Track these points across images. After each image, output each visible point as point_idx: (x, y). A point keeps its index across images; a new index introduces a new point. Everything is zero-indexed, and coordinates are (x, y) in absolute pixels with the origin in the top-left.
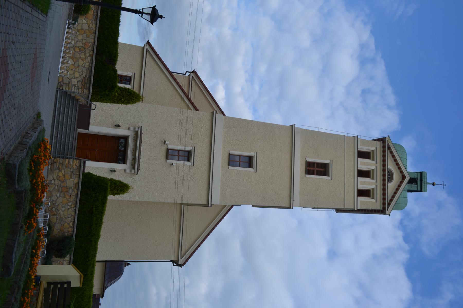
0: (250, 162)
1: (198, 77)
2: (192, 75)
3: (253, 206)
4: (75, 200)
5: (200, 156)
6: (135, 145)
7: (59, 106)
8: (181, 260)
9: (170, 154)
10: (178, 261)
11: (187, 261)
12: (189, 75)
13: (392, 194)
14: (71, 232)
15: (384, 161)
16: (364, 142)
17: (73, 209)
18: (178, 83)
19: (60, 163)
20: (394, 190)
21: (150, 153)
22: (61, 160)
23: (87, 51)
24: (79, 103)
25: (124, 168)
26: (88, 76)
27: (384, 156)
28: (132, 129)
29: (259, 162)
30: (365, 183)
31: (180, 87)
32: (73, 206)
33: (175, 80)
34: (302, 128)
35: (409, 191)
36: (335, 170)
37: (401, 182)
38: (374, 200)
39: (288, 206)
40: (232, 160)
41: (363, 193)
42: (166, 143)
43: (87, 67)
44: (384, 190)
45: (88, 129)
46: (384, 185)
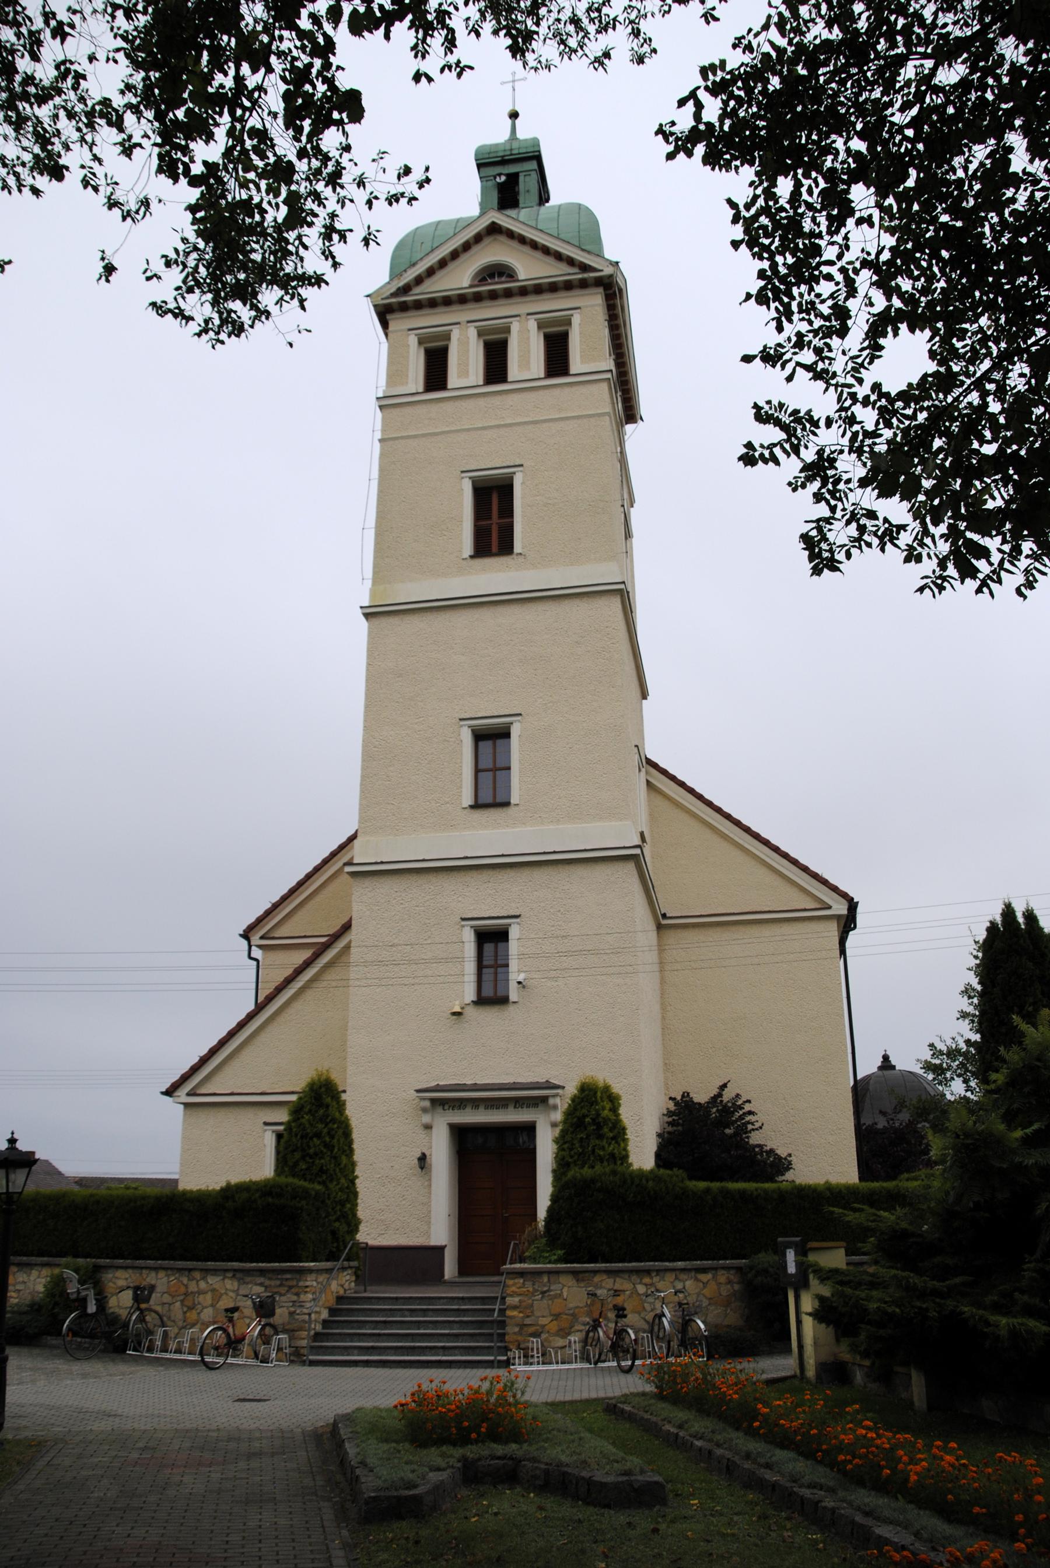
0: (491, 737)
1: (259, 921)
2: (255, 940)
3: (644, 695)
4: (626, 1276)
5: (487, 900)
6: (476, 1103)
7: (356, 1352)
8: (835, 906)
9: (492, 996)
10: (838, 917)
11: (835, 889)
12: (259, 947)
13: (551, 260)
14: (732, 1275)
15: (447, 302)
16: (395, 372)
17: (656, 1279)
18: (288, 981)
19: (520, 1333)
20: (538, 255)
21: (498, 1055)
22: (511, 1329)
23: (193, 1287)
24: (349, 1294)
25: (549, 1127)
26: (262, 1280)
27: (433, 303)
28: (426, 1119)
29: (489, 708)
30: (526, 355)
31: (299, 972)
32: (647, 1280)
33: (279, 990)
34: (369, 584)
35: (544, 197)
36: (490, 460)
37: (511, 234)
38: (576, 319)
39: (616, 603)
40: (491, 796)
41: (557, 361)
42: (457, 1009)
43: (236, 1284)
44: (538, 290)
45: (441, 1249)
46: (523, 292)
